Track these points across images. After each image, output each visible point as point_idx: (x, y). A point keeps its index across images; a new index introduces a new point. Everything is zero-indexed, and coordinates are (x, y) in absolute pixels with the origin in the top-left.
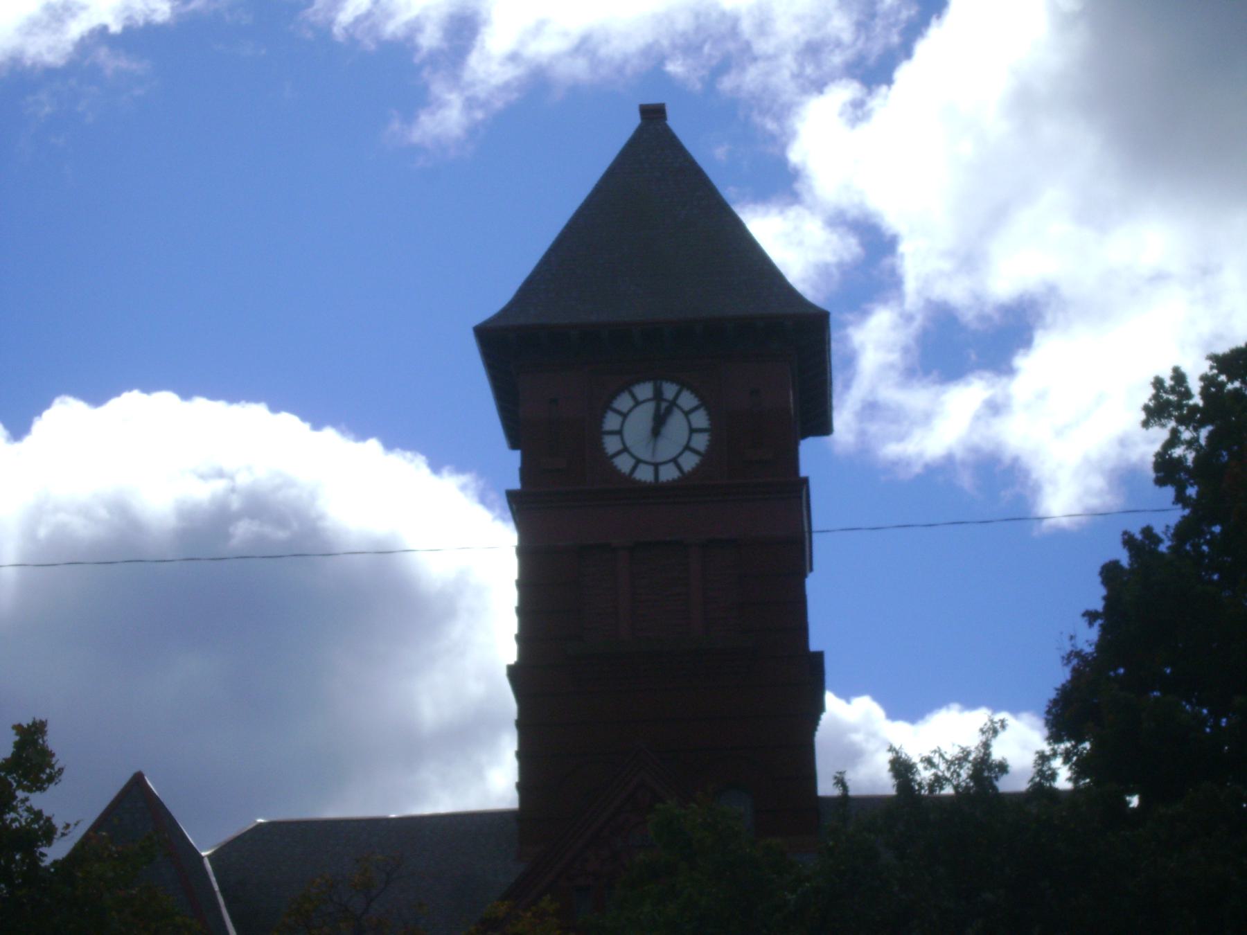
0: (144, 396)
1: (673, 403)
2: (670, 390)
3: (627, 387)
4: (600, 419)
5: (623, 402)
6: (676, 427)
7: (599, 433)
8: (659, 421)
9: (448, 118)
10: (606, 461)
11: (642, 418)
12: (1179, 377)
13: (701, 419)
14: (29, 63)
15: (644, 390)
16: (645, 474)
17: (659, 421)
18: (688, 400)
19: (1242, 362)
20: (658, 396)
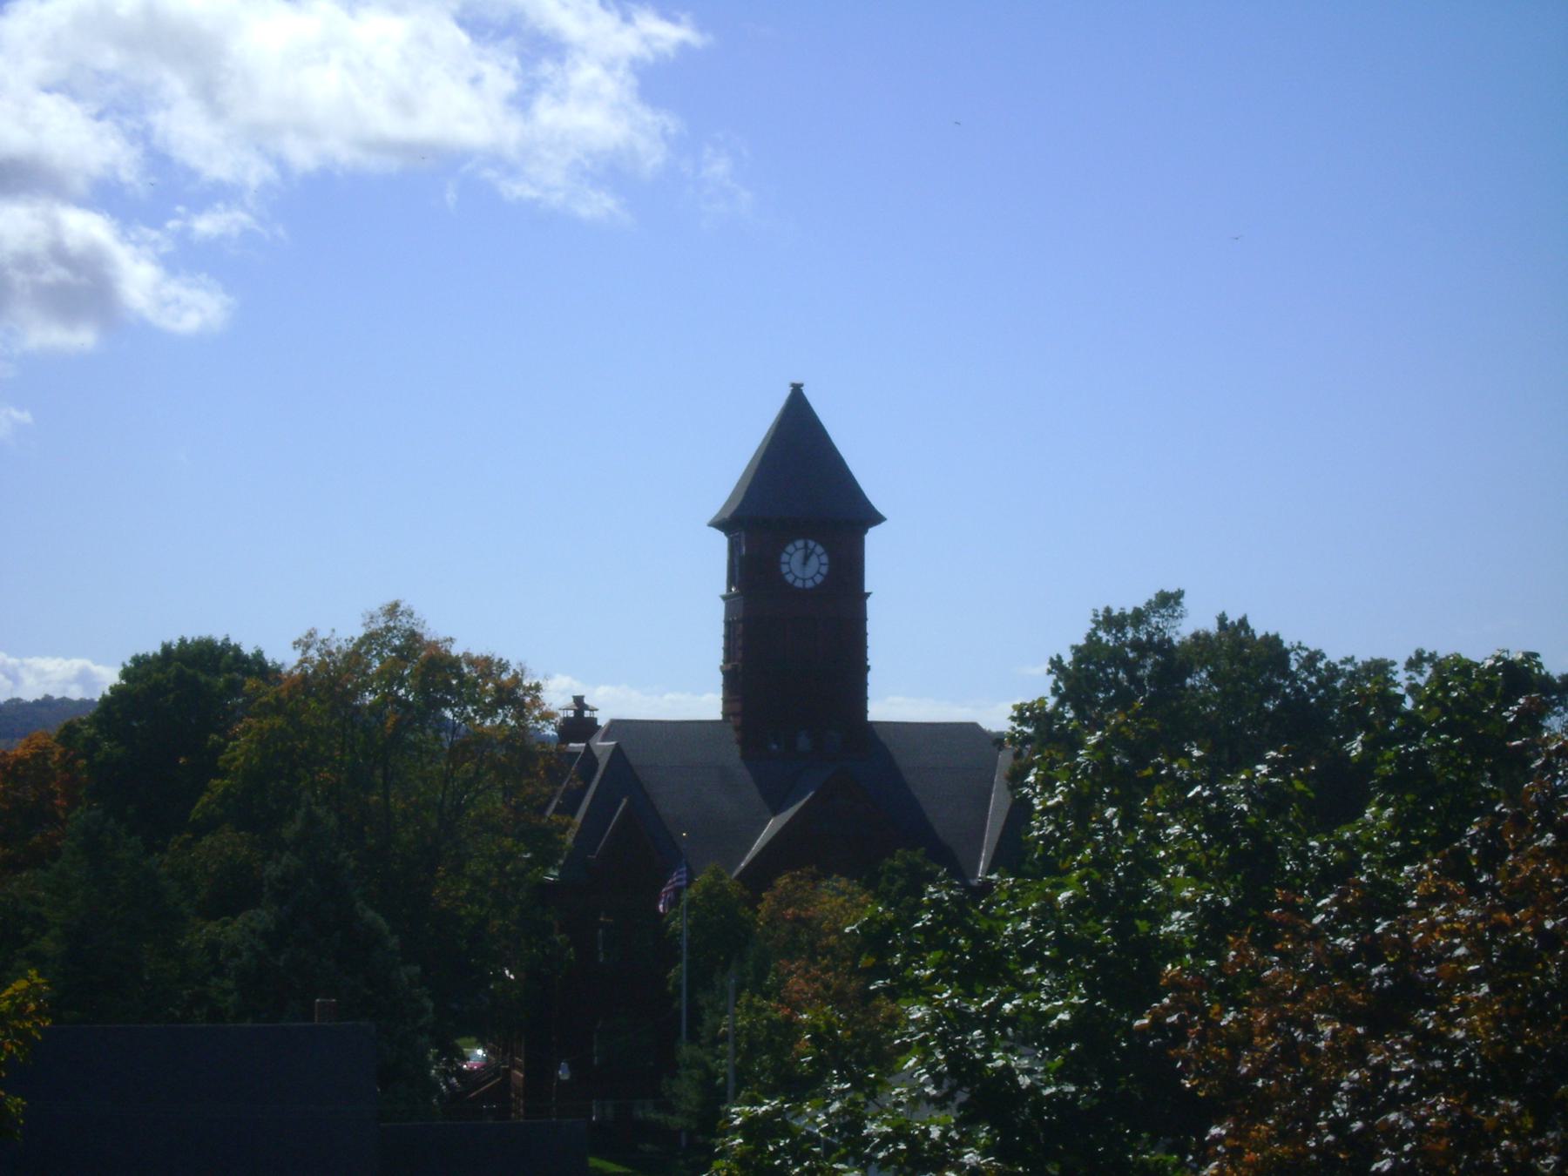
0: (463, 627)
1: (813, 551)
2: (811, 544)
3: (792, 541)
4: (786, 582)
5: (790, 548)
6: (813, 561)
7: (778, 563)
8: (806, 559)
9: (668, 34)
10: (781, 577)
11: (798, 556)
12: (1059, 657)
13: (825, 559)
14: (672, 55)
15: (800, 544)
16: (799, 584)
17: (806, 559)
18: (819, 549)
19: (603, 1)
20: (806, 546)
